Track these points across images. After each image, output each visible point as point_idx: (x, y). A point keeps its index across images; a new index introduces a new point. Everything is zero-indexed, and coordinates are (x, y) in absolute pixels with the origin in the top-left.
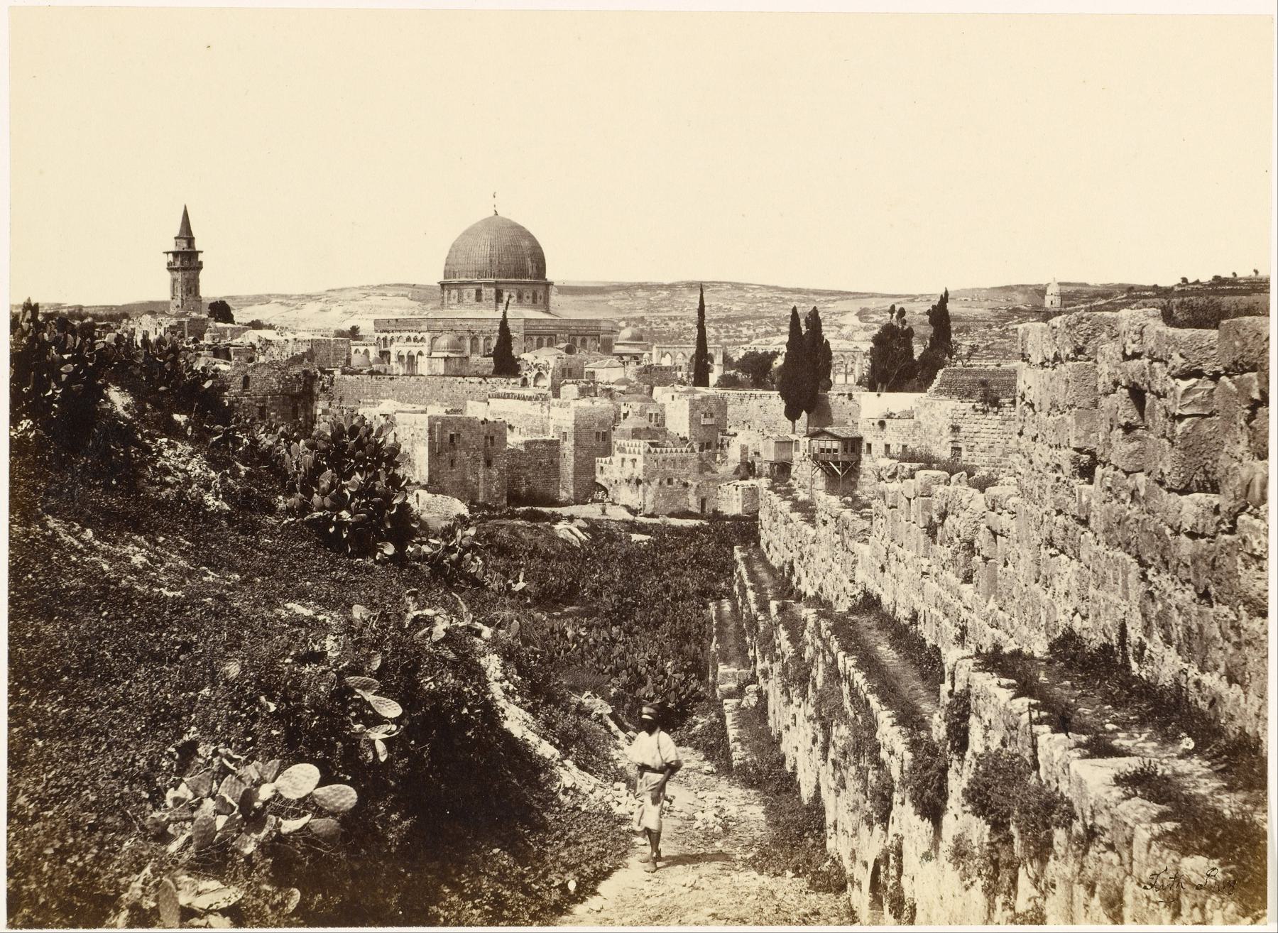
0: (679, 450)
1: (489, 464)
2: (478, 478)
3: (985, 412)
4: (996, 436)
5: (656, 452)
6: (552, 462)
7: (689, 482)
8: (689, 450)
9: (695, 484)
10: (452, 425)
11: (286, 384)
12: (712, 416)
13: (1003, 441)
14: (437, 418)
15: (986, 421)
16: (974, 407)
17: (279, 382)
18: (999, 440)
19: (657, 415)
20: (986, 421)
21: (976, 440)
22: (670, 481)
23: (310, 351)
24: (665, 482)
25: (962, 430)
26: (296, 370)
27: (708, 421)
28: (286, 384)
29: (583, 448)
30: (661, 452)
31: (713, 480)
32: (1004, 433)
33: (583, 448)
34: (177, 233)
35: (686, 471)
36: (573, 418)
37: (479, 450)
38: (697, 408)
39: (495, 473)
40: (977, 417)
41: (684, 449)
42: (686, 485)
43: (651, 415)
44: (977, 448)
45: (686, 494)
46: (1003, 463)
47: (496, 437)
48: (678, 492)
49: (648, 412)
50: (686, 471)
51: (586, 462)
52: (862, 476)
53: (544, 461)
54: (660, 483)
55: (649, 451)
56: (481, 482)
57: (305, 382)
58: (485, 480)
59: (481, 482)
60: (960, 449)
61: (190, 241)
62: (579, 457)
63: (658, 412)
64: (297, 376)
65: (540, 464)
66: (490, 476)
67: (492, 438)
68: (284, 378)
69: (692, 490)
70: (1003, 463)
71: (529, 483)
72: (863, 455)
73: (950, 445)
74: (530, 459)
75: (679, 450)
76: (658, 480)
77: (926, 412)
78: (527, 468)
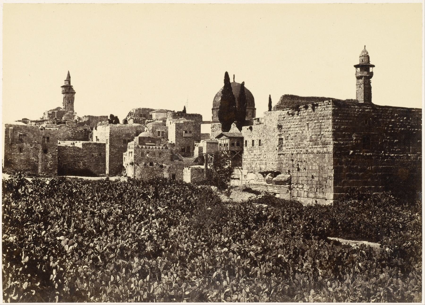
0: (157, 147)
1: (45, 151)
2: (38, 159)
3: (293, 115)
4: (297, 129)
5: (142, 148)
6: (100, 155)
7: (164, 165)
8: (164, 147)
9: (168, 167)
10: (21, 129)
11: (76, 134)
12: (190, 132)
13: (301, 132)
14: (11, 126)
15: (293, 121)
16: (288, 112)
17: (72, 134)
18: (299, 131)
19: (163, 132)
20: (293, 121)
21: (289, 132)
22: (151, 164)
23: (88, 121)
24: (148, 164)
25: (283, 127)
26: (81, 129)
27: (188, 135)
28: (76, 134)
29: (115, 147)
30: (146, 148)
31: (180, 165)
32: (301, 127)
33: (115, 147)
34: (66, 79)
35: (162, 159)
36: (109, 131)
37: (38, 143)
38: (181, 127)
39: (50, 157)
40: (289, 118)
41: (161, 147)
42: (162, 166)
43: (159, 132)
44: (289, 138)
45: (162, 171)
46: (301, 146)
47: (51, 138)
48: (157, 170)
49: (157, 130)
50: (162, 159)
51: (118, 155)
52: (243, 160)
53: (96, 154)
54: (145, 165)
55: (138, 147)
56: (40, 160)
57: (85, 133)
58: (42, 160)
59: (40, 160)
60: (282, 139)
61: (69, 83)
62: (113, 152)
63: (164, 130)
64: (81, 131)
65: (93, 156)
66: (46, 158)
67: (48, 138)
68: (75, 132)
69: (166, 170)
70: (301, 146)
71: (85, 165)
72: (244, 147)
73: (278, 137)
74: (85, 152)
75: (157, 147)
76: (144, 163)
77: (268, 118)
78: (84, 157)
